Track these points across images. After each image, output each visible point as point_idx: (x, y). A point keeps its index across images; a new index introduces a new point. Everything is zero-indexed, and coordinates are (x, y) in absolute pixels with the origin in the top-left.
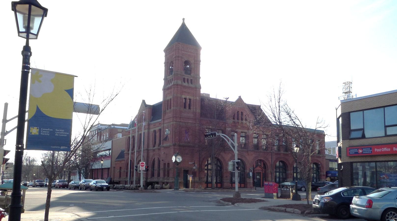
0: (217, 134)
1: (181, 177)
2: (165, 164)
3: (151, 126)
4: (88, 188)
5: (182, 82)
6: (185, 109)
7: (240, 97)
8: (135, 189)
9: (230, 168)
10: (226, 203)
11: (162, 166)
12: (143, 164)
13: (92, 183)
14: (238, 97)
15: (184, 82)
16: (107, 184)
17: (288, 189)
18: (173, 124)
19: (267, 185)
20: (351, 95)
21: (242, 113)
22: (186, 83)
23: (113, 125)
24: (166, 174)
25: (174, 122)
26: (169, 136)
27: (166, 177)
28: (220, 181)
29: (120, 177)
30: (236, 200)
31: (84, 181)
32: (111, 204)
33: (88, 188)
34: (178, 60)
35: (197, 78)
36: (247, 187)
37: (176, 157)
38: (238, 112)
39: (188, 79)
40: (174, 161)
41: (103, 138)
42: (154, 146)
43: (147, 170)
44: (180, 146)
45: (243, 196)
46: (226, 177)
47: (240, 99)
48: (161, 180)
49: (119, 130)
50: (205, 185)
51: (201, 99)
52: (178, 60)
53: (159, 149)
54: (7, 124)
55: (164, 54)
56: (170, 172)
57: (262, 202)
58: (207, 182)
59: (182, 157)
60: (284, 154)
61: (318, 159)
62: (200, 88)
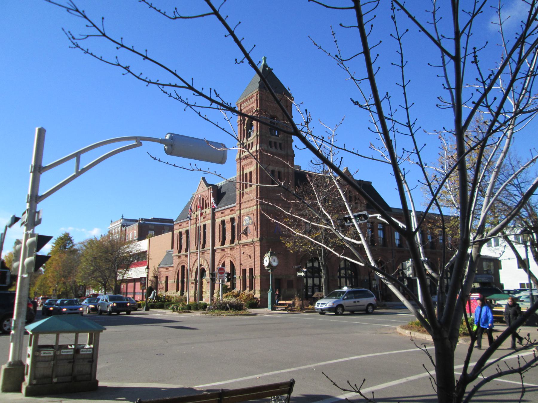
2: (245, 270)
3: (218, 215)
5: (267, 147)
15: (271, 147)
22: (274, 148)
23: (142, 219)
24: (248, 284)
29: (167, 290)
39: (275, 143)
49: (150, 227)
54: (44, 176)
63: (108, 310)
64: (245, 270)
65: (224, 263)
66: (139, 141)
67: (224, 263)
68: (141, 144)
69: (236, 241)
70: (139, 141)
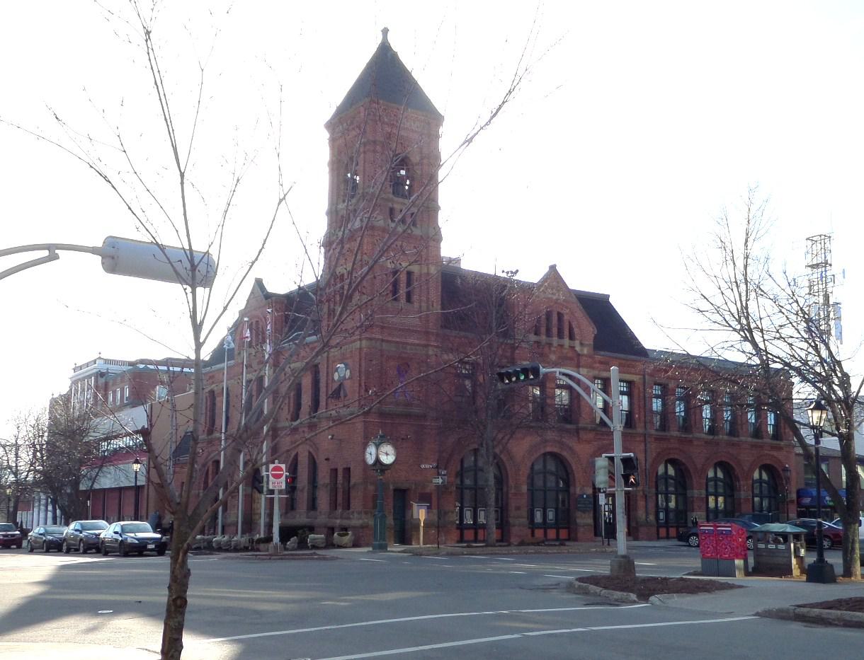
0: (543, 370)
1: (389, 512)
2: (334, 471)
4: (95, 547)
6: (395, 304)
7: (553, 268)
8: (246, 549)
9: (601, 478)
10: (618, 594)
11: (324, 477)
12: (281, 469)
13: (108, 531)
14: (547, 270)
16: (158, 536)
17: (782, 547)
18: (361, 349)
19: (709, 534)
20: (828, 273)
21: (560, 316)
23: (142, 361)
25: (364, 343)
26: (347, 384)
27: (340, 510)
28: (562, 517)
30: (626, 582)
31: (78, 527)
32: (245, 604)
33: (95, 547)
34: (375, 151)
35: (428, 209)
36: (576, 540)
37: (377, 446)
38: (549, 315)
40: (370, 460)
41: (114, 398)
42: (296, 416)
43: (292, 487)
44: (382, 414)
45: (646, 567)
46: (518, 508)
47: (553, 276)
48: (322, 518)
50: (455, 534)
51: (442, 273)
52: (375, 151)
53: (312, 427)
55: (326, 135)
56: (353, 494)
57: (730, 592)
58: (461, 527)
59: (396, 448)
60: (681, 440)
61: (775, 453)
62: (436, 238)
63: (637, 575)
64: (336, 470)
65: (296, 455)
66: (52, 252)
67: (296, 455)
68: (56, 257)
69: (322, 410)
70: (52, 252)
